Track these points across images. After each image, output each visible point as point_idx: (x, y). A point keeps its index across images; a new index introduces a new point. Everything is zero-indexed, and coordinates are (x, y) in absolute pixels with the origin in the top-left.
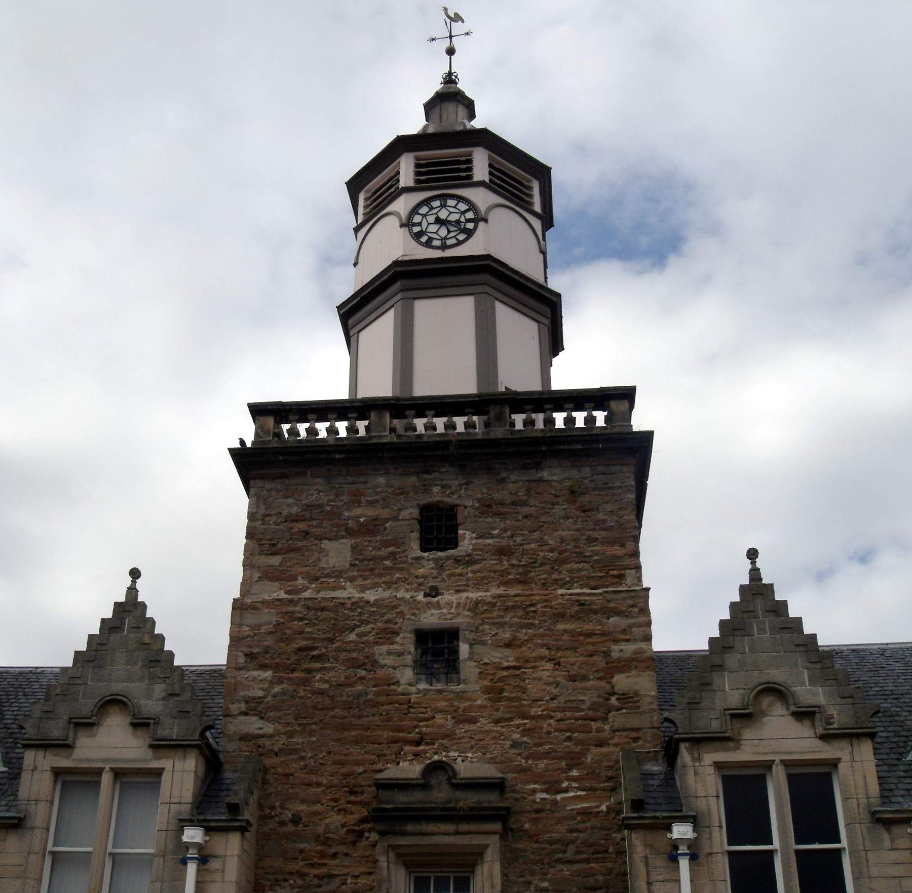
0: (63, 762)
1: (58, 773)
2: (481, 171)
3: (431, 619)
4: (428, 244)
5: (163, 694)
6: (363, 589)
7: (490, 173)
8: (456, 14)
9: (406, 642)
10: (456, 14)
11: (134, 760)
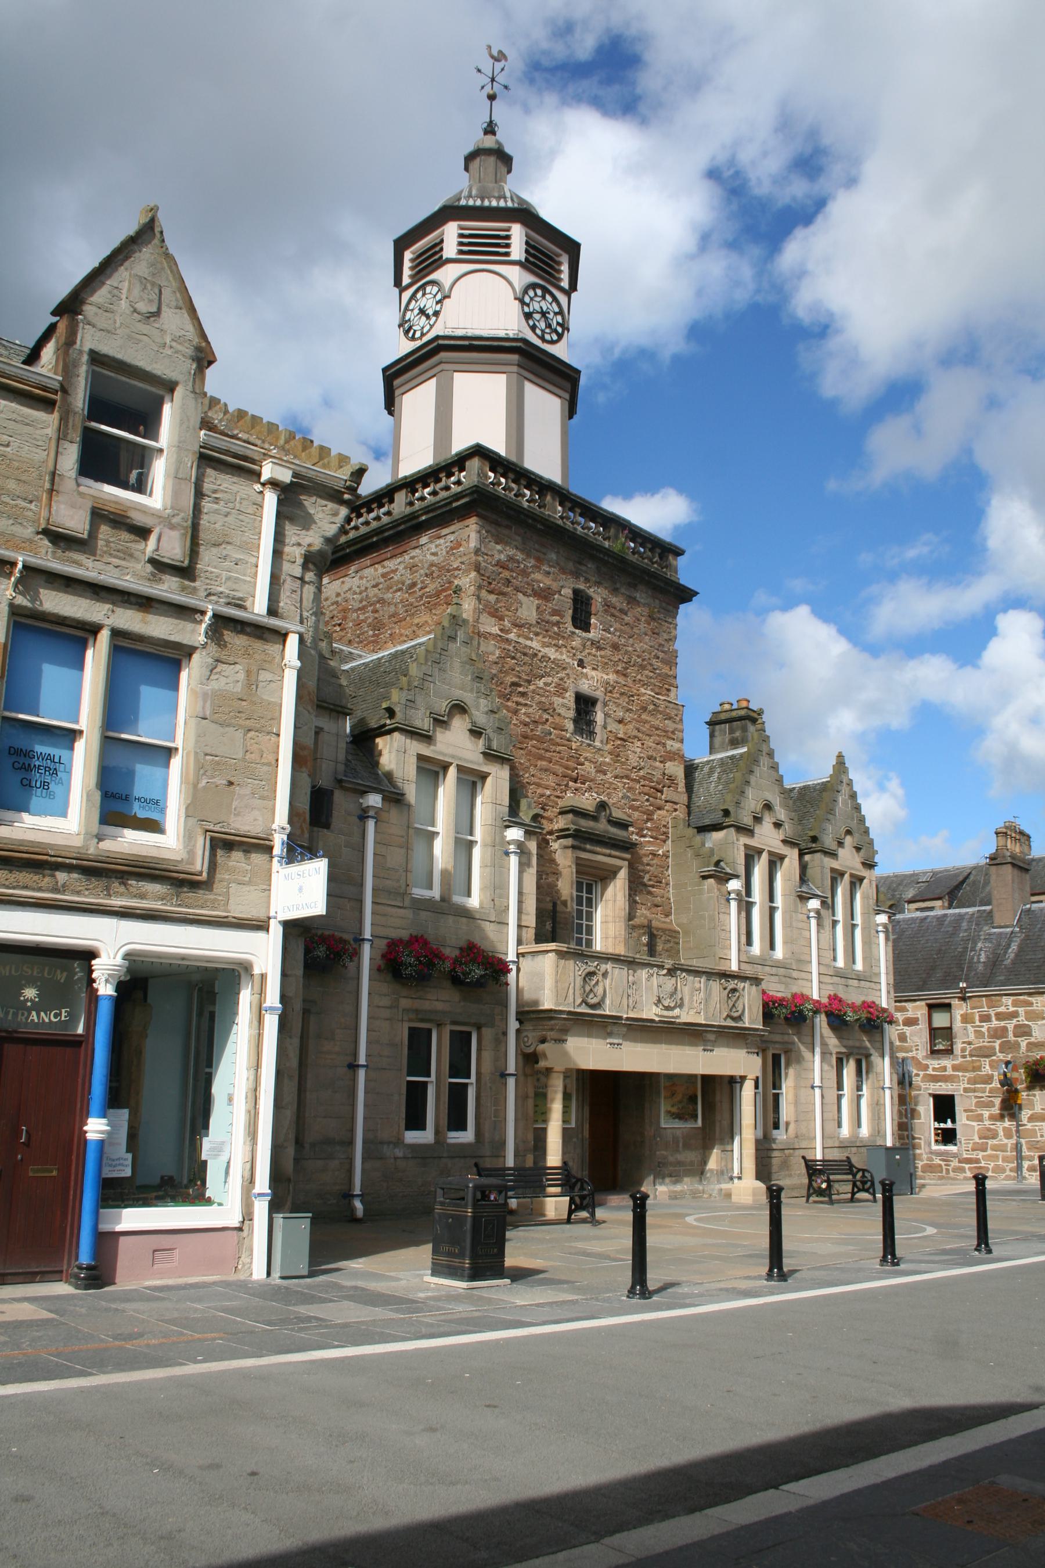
0: (426, 751)
1: (421, 758)
2: (517, 250)
5: (486, 709)
6: (545, 645)
7: (527, 251)
8: (500, 52)
9: (570, 698)
10: (500, 52)
11: (471, 762)
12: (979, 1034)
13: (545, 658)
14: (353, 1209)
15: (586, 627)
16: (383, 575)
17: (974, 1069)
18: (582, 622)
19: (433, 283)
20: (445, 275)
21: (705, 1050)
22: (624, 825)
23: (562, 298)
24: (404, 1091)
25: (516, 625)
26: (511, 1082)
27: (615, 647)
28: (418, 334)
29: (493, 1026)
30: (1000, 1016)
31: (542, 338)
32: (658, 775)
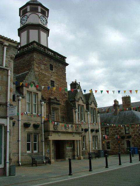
1: (27, 91)
3: (52, 79)
4: (42, 23)
9: (50, 81)
12: (113, 132)
13: (46, 75)
14: (19, 164)
15: (52, 70)
16: (19, 62)
17: (113, 137)
18: (51, 69)
19: (26, 15)
20: (28, 14)
21: (73, 136)
22: (59, 101)
23: (46, 18)
24: (27, 144)
25: (41, 70)
26: (43, 142)
27: (56, 73)
28: (23, 24)
29: (40, 134)
30: (116, 129)
31: (43, 24)
32: (63, 93)
